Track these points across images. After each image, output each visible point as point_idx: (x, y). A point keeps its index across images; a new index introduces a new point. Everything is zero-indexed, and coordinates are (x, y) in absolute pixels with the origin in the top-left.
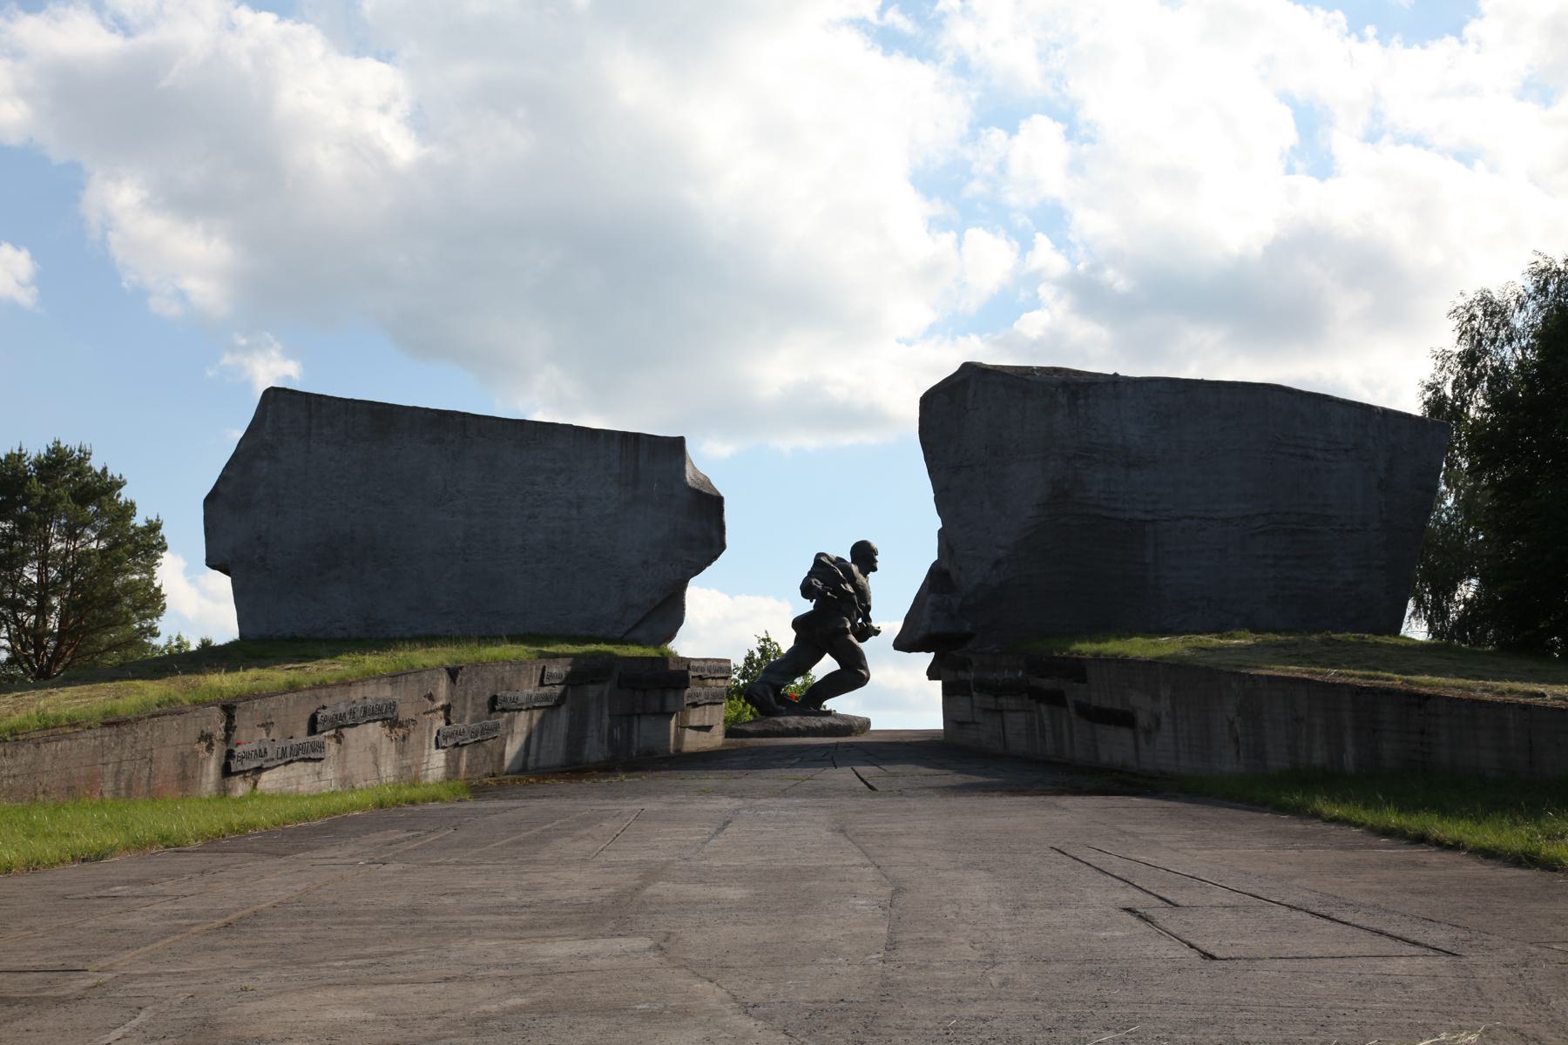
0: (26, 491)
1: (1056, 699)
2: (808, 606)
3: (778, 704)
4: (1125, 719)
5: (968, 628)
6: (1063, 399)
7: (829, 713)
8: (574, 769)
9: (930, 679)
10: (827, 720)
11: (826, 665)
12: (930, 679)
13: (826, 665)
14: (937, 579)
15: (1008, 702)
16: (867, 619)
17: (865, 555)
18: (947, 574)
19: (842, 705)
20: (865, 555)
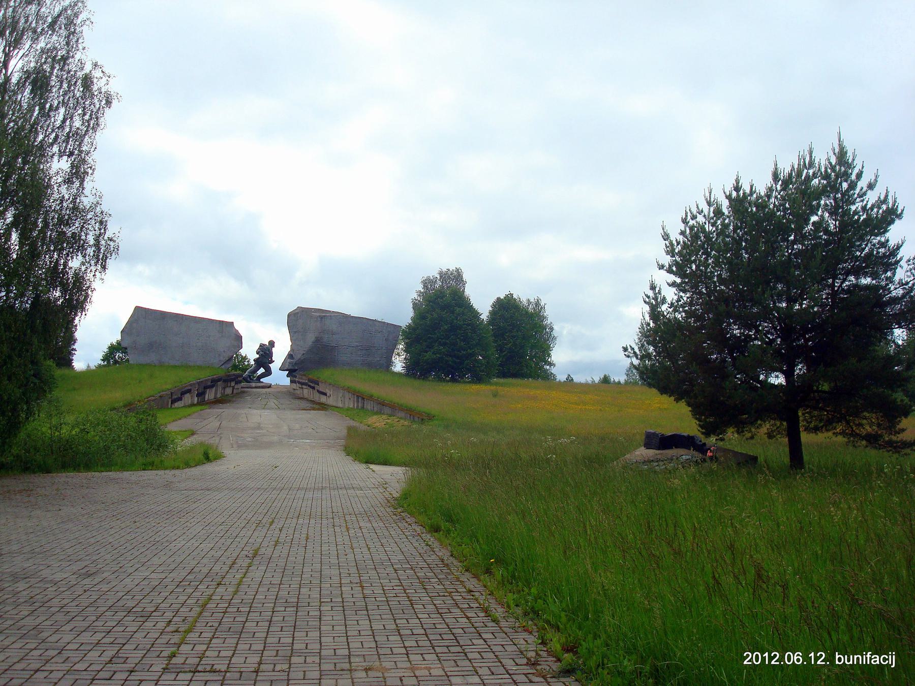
0: (246, 363)
1: (313, 388)
2: (258, 356)
3: (707, 434)
4: (325, 394)
5: (296, 368)
6: (319, 319)
7: (262, 382)
8: (473, 383)
9: (138, 309)
10: (262, 384)
11: (262, 370)
12: (138, 309)
13: (262, 370)
14: (290, 356)
15: (304, 386)
16: (272, 359)
17: (272, 344)
18: (292, 355)
19: (265, 380)
20: (272, 344)
